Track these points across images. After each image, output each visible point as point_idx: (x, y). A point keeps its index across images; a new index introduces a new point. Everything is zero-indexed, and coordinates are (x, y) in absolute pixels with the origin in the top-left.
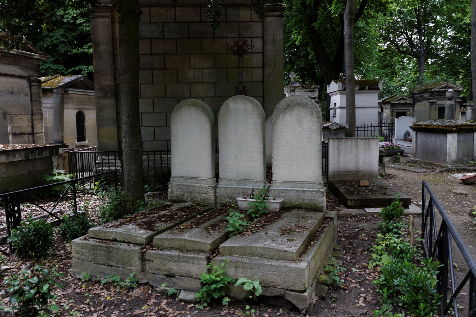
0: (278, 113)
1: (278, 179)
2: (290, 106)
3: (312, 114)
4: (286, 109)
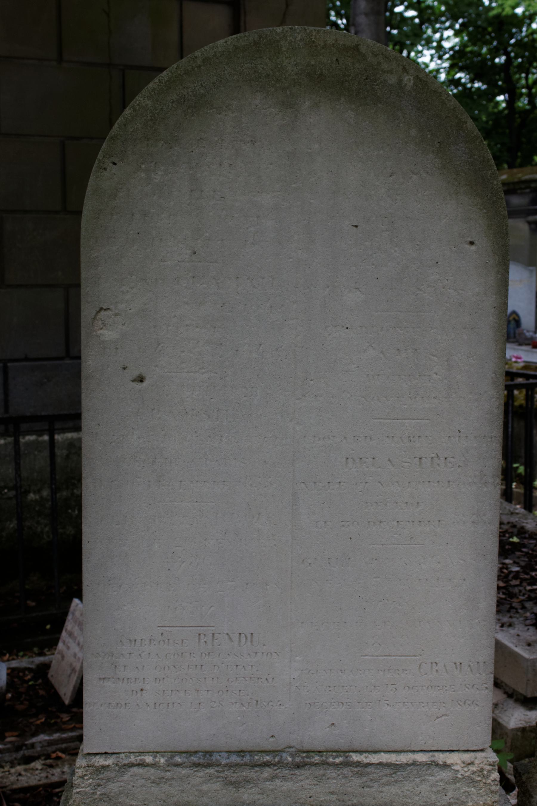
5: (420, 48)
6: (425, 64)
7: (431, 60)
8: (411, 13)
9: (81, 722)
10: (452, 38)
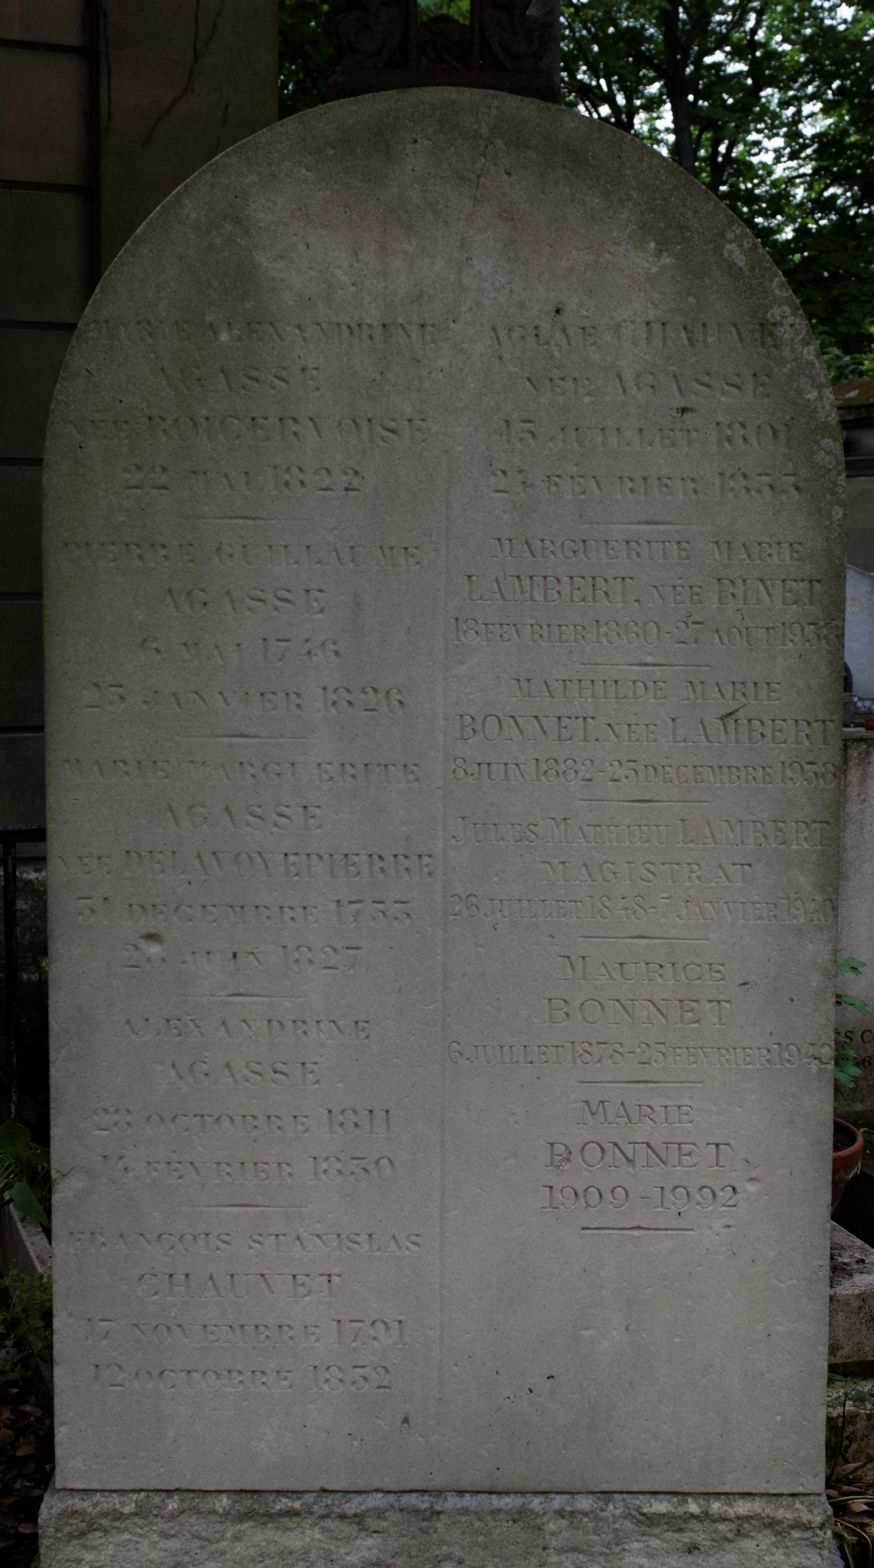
5: (753, 137)
6: (764, 165)
7: (777, 160)
8: (736, 67)
9: (836, 1123)
10: (820, 116)
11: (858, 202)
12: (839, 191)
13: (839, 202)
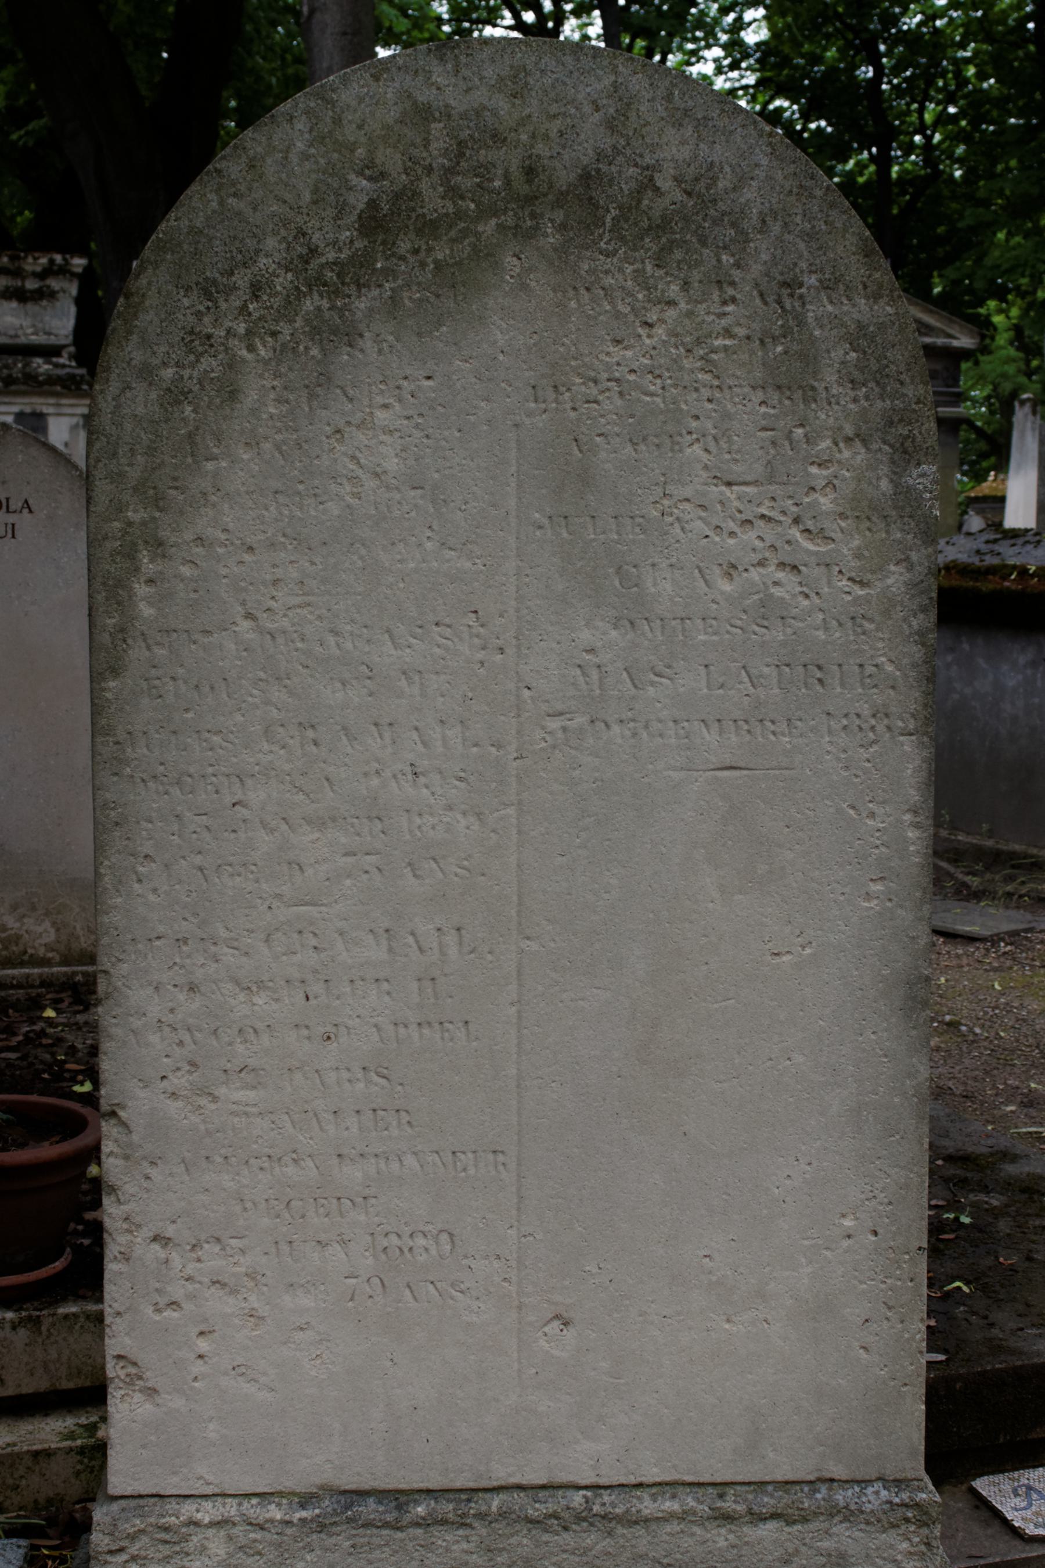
0: (198, 343)
1: (204, 1474)
2: (430, 228)
3: (792, 380)
4: (354, 273)
7: (719, 71)
11: (806, 116)
12: (786, 104)
13: (787, 114)
